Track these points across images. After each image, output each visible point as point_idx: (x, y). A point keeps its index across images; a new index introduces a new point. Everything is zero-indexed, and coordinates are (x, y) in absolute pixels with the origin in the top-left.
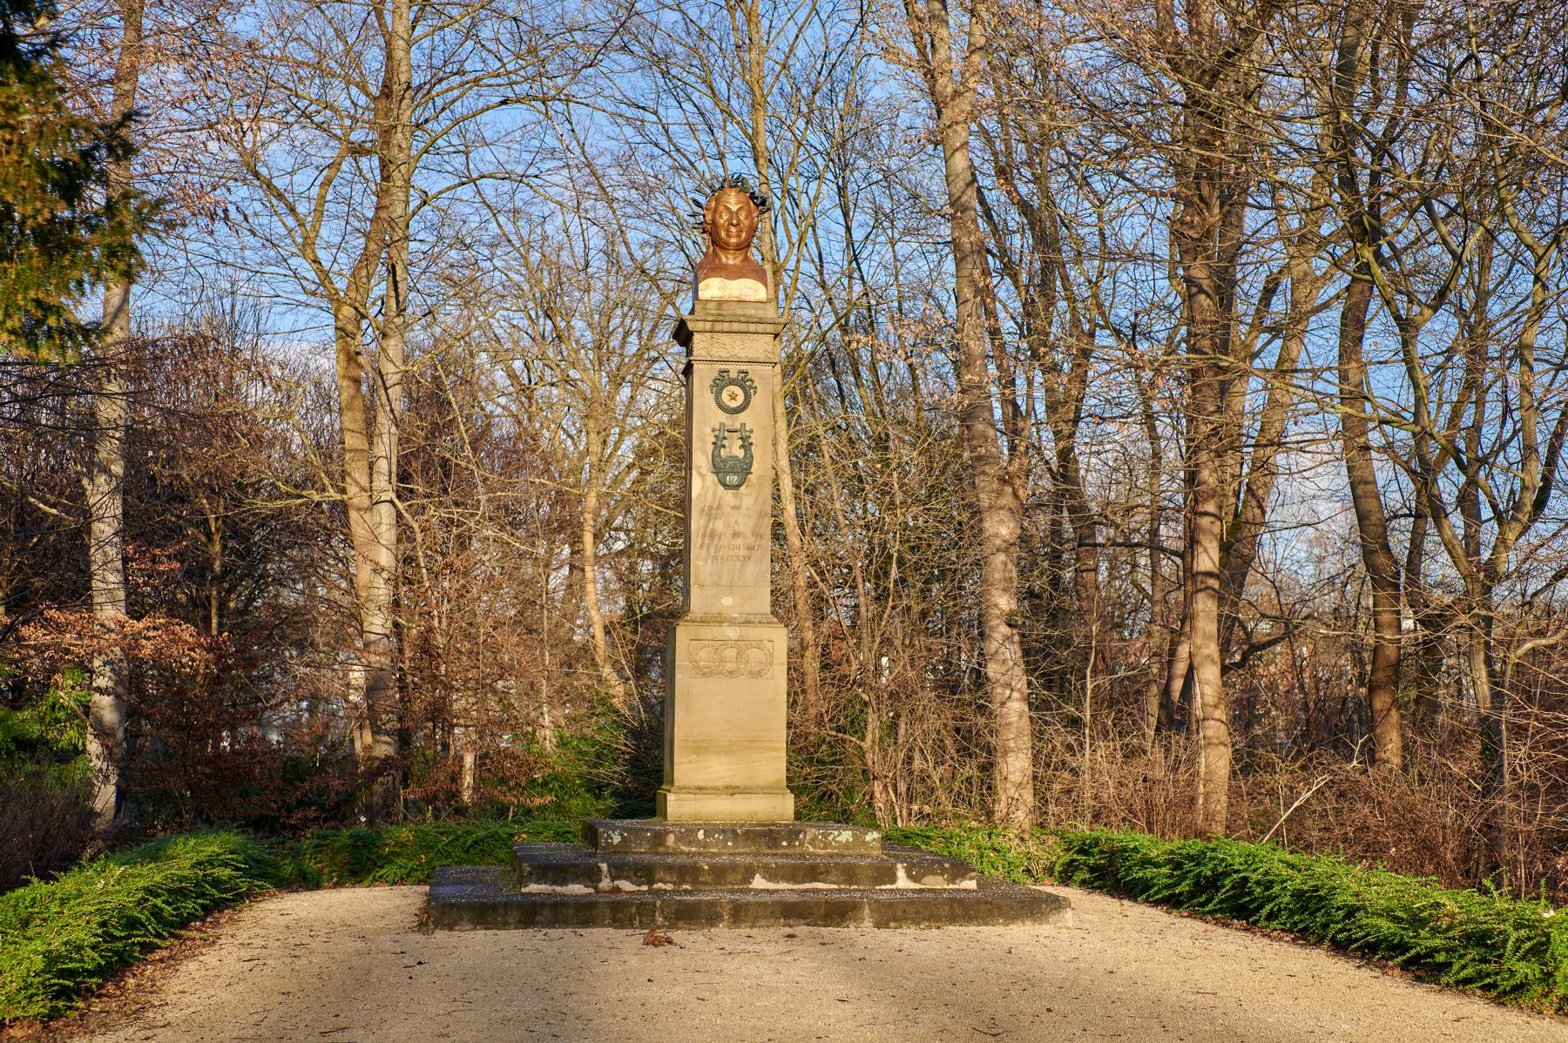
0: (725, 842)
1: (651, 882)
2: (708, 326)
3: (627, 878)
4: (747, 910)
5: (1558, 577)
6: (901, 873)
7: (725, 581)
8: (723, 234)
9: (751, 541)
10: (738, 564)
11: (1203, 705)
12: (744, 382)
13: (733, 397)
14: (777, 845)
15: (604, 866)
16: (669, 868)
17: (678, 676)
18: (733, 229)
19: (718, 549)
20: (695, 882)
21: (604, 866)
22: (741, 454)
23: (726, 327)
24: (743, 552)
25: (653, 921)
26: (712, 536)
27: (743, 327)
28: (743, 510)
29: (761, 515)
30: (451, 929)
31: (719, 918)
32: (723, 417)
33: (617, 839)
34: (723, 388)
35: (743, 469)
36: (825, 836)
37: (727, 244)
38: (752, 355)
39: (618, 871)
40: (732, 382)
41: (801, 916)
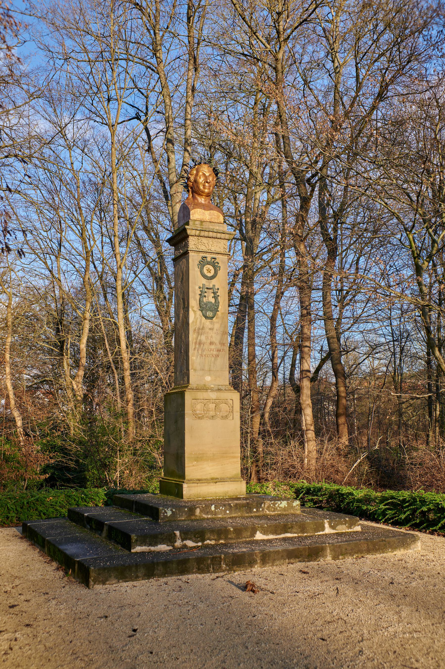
0: (225, 511)
1: (203, 540)
2: (198, 232)
3: (190, 539)
4: (269, 556)
6: (327, 525)
7: (207, 368)
8: (201, 187)
9: (219, 347)
10: (213, 359)
11: (306, 424)
12: (214, 264)
13: (209, 271)
14: (251, 511)
15: (178, 533)
16: (212, 531)
17: (187, 419)
18: (207, 184)
19: (203, 350)
20: (226, 538)
21: (178, 533)
22: (213, 301)
23: (206, 234)
24: (215, 353)
25: (220, 567)
26: (200, 343)
27: (215, 235)
28: (215, 330)
30: (104, 584)
31: (255, 562)
32: (204, 281)
33: (169, 513)
34: (204, 266)
35: (215, 308)
36: (274, 504)
37: (203, 192)
38: (218, 250)
39: (185, 535)
40: (208, 263)
41: (296, 557)
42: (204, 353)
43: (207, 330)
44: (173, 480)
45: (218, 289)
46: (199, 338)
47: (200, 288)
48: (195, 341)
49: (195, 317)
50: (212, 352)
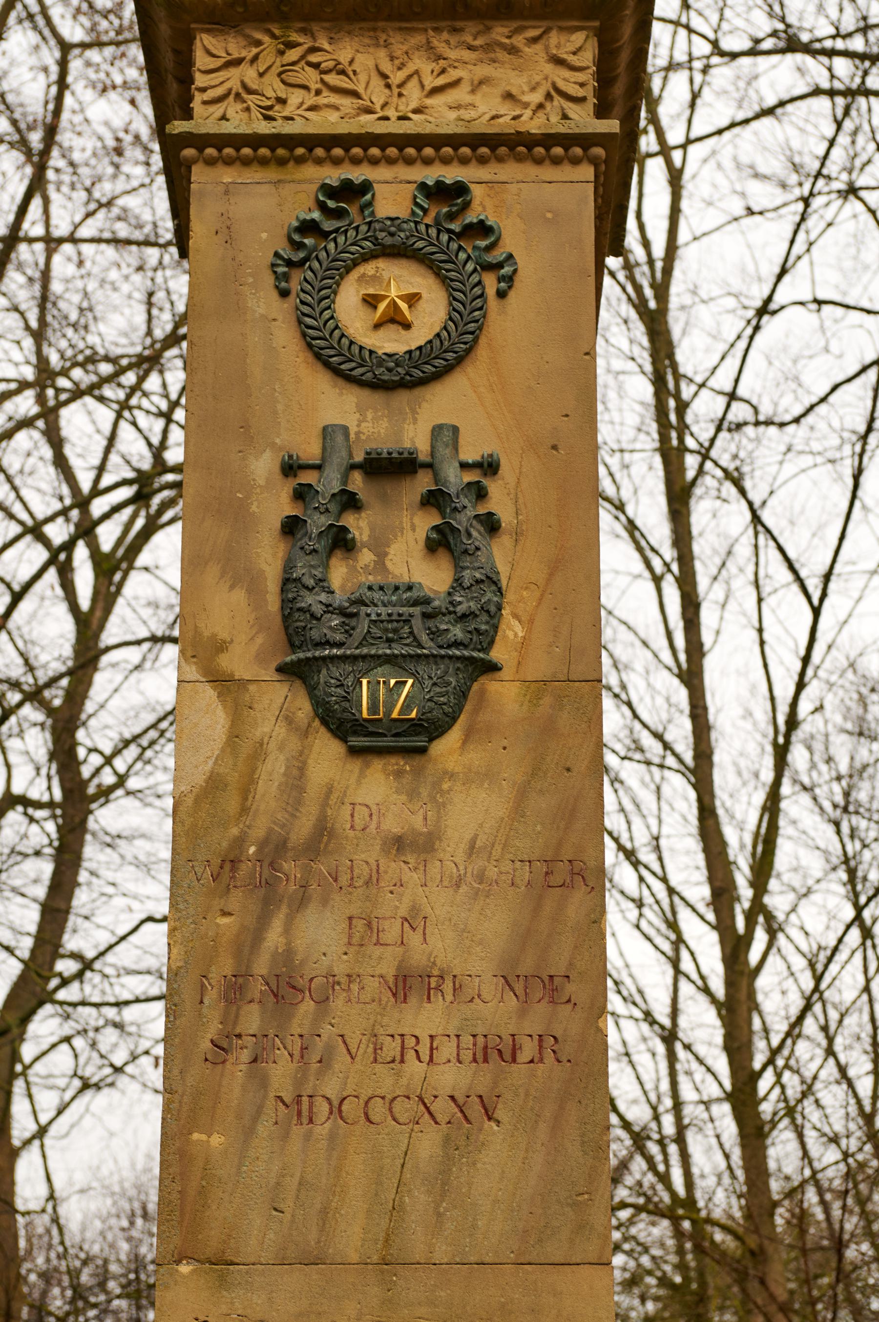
5: (765, 1315)
7: (352, 1237)
9: (497, 1012)
10: (428, 1144)
19: (311, 1057)
22: (434, 578)
24: (451, 1078)
26: (285, 989)
28: (453, 848)
29: (618, 707)
42: (331, 1088)
43: (367, 855)
44: (677, 506)
45: (489, 467)
46: (274, 937)
47: (290, 468)
48: (225, 966)
49: (234, 736)
50: (414, 1068)
